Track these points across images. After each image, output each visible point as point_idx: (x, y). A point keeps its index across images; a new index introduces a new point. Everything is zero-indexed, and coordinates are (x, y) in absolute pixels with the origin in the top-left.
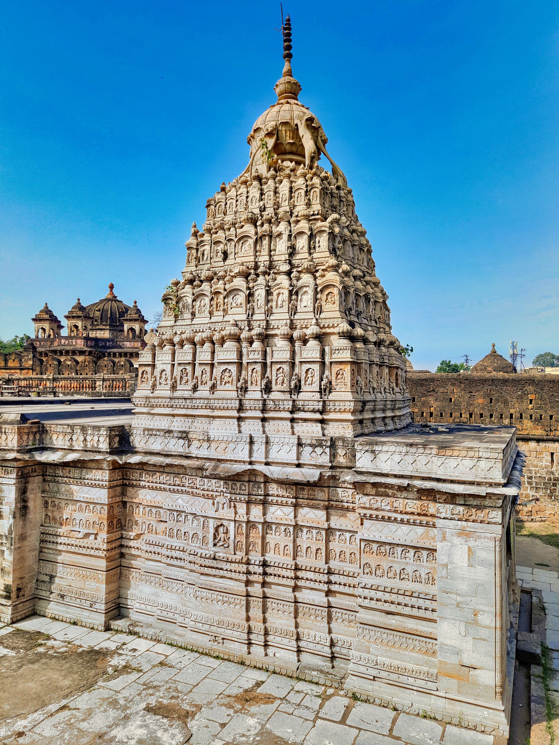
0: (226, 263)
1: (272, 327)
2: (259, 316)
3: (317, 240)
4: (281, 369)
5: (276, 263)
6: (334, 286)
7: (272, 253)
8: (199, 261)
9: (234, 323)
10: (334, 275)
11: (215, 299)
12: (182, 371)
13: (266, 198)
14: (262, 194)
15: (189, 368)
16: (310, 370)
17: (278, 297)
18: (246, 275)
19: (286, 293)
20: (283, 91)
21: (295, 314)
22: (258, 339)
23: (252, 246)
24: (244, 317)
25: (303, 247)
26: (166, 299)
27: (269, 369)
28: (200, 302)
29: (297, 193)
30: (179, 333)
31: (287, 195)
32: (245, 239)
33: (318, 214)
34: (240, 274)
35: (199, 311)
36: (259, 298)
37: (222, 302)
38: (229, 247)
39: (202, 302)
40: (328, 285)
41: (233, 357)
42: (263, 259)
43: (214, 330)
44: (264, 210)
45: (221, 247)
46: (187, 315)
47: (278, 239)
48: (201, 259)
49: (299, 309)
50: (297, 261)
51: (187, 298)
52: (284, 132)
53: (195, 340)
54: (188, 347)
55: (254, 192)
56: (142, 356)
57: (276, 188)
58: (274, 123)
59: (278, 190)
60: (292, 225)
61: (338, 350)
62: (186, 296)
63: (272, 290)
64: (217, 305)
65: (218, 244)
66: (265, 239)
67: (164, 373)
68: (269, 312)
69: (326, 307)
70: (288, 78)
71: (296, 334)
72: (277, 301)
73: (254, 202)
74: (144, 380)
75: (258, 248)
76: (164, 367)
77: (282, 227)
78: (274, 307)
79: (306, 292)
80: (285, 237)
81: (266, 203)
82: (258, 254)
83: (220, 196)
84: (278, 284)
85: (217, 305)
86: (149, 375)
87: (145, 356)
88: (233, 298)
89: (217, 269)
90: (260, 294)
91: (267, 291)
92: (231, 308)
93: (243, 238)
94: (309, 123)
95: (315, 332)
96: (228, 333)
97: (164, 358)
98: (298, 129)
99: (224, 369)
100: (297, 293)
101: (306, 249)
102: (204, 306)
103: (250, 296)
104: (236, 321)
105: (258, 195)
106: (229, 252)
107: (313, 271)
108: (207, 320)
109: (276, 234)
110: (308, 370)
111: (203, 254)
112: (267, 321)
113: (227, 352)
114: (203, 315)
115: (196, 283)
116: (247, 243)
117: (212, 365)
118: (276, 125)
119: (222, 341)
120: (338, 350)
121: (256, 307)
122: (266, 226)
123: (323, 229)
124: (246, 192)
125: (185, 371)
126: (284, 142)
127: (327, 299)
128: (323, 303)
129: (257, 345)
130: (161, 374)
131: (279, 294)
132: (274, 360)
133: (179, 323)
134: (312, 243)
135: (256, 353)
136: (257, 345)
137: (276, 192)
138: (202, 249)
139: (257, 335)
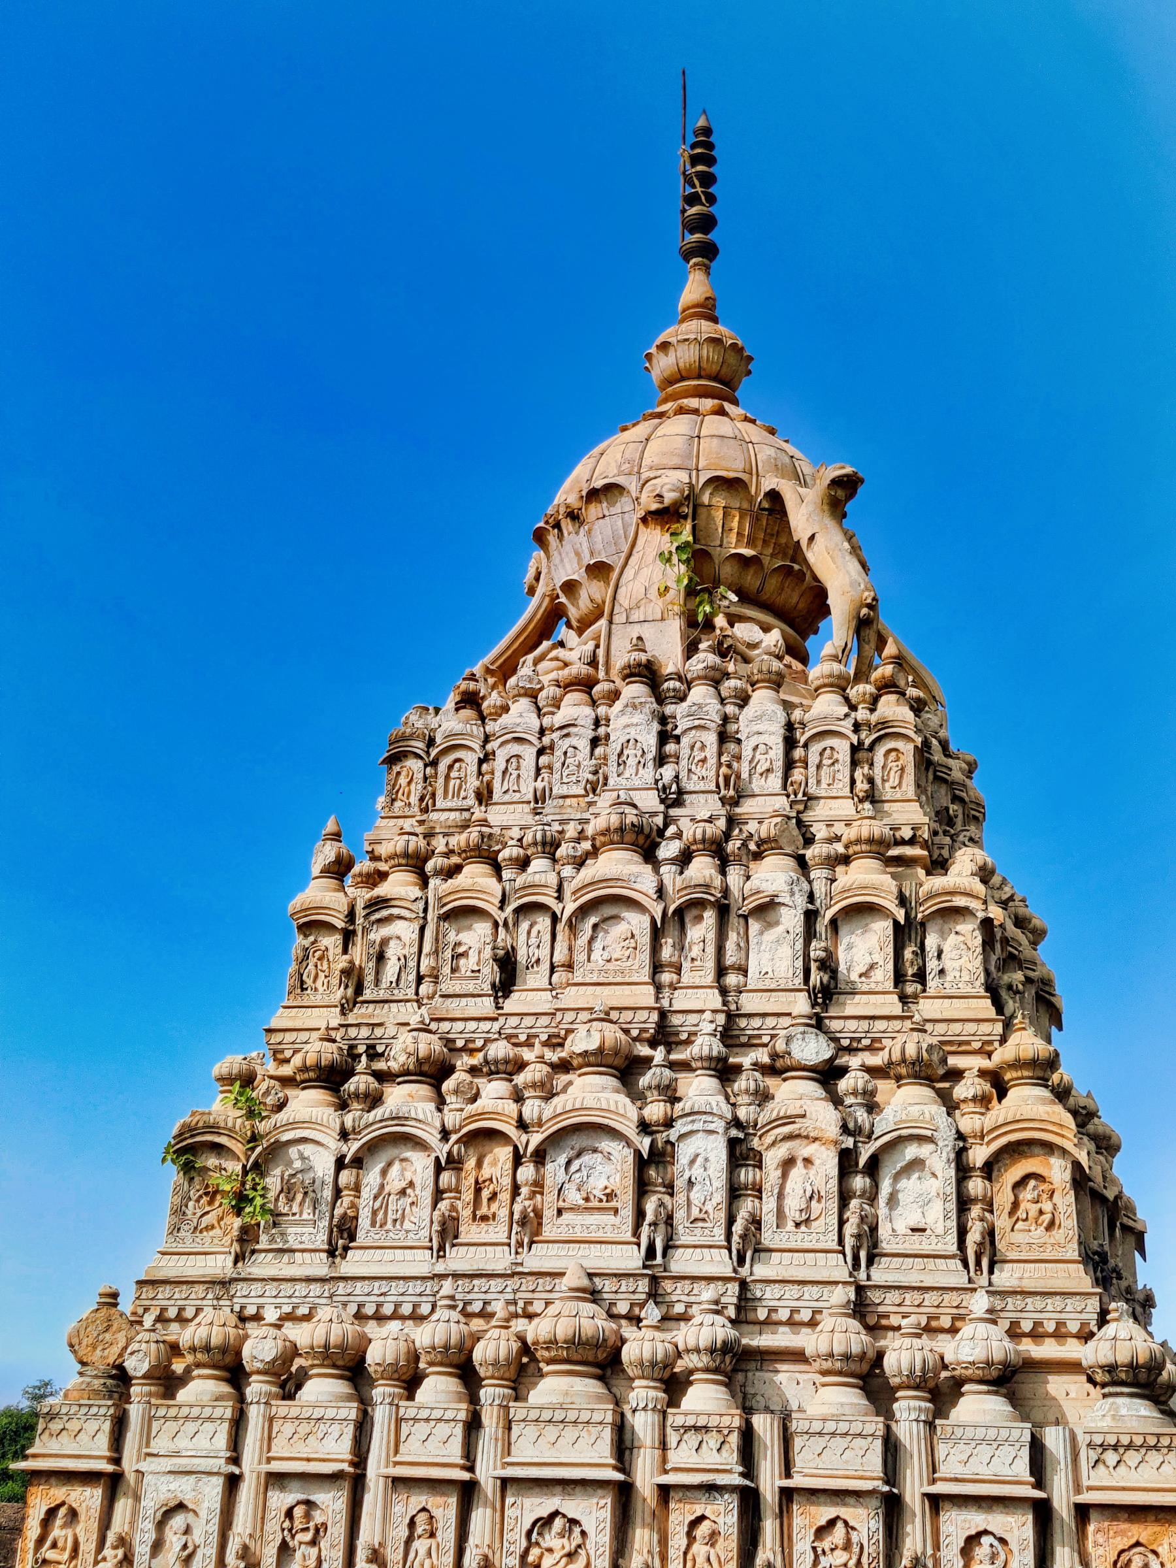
0: (509, 1005)
1: (762, 1314)
2: (701, 1257)
3: (931, 941)
4: (840, 1527)
5: (756, 1023)
6: (1049, 1148)
7: (732, 979)
8: (359, 990)
9: (585, 1282)
10: (1044, 1101)
11: (471, 1163)
12: (289, 1514)
13: (685, 752)
14: (664, 737)
15: (332, 1504)
16: (986, 1540)
17: (785, 1176)
18: (627, 1069)
19: (827, 1162)
20: (689, 370)
21: (870, 1262)
22: (716, 1371)
23: (645, 940)
24: (632, 1258)
25: (872, 967)
26: (191, 1150)
27: (769, 1527)
28: (384, 1173)
29: (815, 748)
30: (271, 1315)
31: (777, 752)
32: (608, 911)
33: (912, 842)
34: (598, 1059)
35: (375, 1213)
36: (697, 1172)
37: (507, 1181)
38: (522, 937)
39: (396, 1167)
40: (1020, 1143)
41: (592, 1453)
42: (696, 1002)
43: (485, 1315)
44: (678, 803)
45: (475, 937)
46: (308, 1231)
47: (754, 926)
48: (369, 979)
49: (887, 1243)
50: (852, 1025)
51: (307, 1149)
52: (719, 515)
53: (477, 1355)
54: (323, 1390)
55: (631, 722)
56: (55, 1426)
57: (726, 719)
58: (683, 476)
59: (732, 728)
60: (813, 875)
61: (1115, 1447)
62: (304, 1140)
63: (755, 1143)
64: (478, 1191)
65: (465, 922)
66: (699, 918)
67: (178, 1522)
68: (748, 1246)
69: (1016, 1239)
70: (706, 328)
71: (901, 1356)
72: (781, 1196)
73: (632, 762)
74: (51, 1555)
75: (667, 953)
76: (183, 1489)
77: (771, 875)
78: (769, 1219)
79: (917, 1164)
80: (791, 919)
81: (683, 775)
82: (666, 977)
83: (451, 722)
84: (789, 1119)
85: (478, 1191)
86: (86, 1530)
87: (74, 1425)
88: (569, 1163)
89: (459, 1026)
90: (702, 1157)
91: (733, 1143)
92: (560, 1212)
93: (606, 904)
94: (841, 494)
95: (998, 1356)
96: (563, 1330)
97: (182, 1443)
98: (783, 513)
99: (545, 1514)
100: (873, 1168)
101: (884, 976)
102: (403, 1192)
103: (652, 1164)
104: (591, 1276)
105: (650, 741)
106: (521, 956)
107: (933, 1072)
108: (421, 1263)
109: (751, 904)
110: (973, 1540)
111: (381, 958)
112: (744, 1285)
113: (561, 1432)
114: (395, 1236)
115: (360, 1082)
116: (618, 930)
117: (468, 1492)
118: (691, 487)
119: (522, 1369)
120: (1115, 1447)
121: (679, 1216)
122: (702, 868)
123: (960, 901)
124: (589, 722)
125: (308, 1516)
126: (716, 552)
127: (1016, 1205)
128: (1002, 1222)
129: (704, 1398)
130: (161, 1525)
131: (788, 1164)
132: (797, 1481)
133: (263, 1265)
134: (908, 954)
135: (712, 1440)
136: (704, 1398)
137: (724, 737)
138: (376, 935)
139: (712, 1351)
